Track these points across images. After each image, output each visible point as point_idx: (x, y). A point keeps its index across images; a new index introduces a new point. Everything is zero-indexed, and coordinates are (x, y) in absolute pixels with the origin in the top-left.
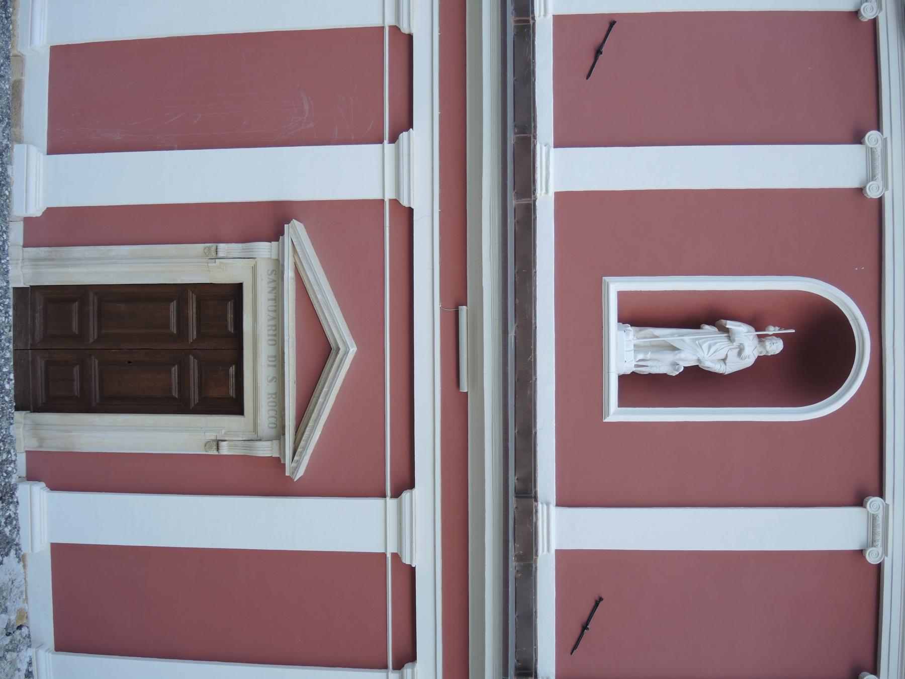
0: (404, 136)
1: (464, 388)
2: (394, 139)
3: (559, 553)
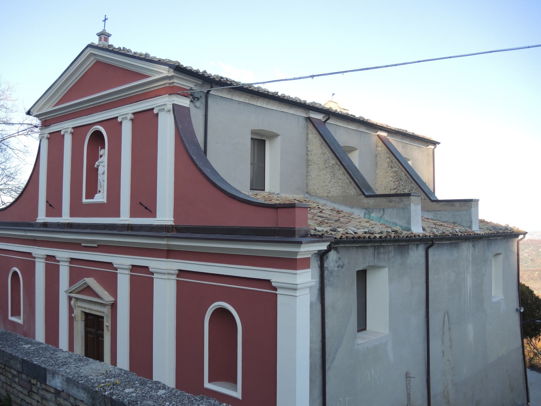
0: (115, 266)
1: (96, 245)
2: (275, 289)
3: (131, 217)
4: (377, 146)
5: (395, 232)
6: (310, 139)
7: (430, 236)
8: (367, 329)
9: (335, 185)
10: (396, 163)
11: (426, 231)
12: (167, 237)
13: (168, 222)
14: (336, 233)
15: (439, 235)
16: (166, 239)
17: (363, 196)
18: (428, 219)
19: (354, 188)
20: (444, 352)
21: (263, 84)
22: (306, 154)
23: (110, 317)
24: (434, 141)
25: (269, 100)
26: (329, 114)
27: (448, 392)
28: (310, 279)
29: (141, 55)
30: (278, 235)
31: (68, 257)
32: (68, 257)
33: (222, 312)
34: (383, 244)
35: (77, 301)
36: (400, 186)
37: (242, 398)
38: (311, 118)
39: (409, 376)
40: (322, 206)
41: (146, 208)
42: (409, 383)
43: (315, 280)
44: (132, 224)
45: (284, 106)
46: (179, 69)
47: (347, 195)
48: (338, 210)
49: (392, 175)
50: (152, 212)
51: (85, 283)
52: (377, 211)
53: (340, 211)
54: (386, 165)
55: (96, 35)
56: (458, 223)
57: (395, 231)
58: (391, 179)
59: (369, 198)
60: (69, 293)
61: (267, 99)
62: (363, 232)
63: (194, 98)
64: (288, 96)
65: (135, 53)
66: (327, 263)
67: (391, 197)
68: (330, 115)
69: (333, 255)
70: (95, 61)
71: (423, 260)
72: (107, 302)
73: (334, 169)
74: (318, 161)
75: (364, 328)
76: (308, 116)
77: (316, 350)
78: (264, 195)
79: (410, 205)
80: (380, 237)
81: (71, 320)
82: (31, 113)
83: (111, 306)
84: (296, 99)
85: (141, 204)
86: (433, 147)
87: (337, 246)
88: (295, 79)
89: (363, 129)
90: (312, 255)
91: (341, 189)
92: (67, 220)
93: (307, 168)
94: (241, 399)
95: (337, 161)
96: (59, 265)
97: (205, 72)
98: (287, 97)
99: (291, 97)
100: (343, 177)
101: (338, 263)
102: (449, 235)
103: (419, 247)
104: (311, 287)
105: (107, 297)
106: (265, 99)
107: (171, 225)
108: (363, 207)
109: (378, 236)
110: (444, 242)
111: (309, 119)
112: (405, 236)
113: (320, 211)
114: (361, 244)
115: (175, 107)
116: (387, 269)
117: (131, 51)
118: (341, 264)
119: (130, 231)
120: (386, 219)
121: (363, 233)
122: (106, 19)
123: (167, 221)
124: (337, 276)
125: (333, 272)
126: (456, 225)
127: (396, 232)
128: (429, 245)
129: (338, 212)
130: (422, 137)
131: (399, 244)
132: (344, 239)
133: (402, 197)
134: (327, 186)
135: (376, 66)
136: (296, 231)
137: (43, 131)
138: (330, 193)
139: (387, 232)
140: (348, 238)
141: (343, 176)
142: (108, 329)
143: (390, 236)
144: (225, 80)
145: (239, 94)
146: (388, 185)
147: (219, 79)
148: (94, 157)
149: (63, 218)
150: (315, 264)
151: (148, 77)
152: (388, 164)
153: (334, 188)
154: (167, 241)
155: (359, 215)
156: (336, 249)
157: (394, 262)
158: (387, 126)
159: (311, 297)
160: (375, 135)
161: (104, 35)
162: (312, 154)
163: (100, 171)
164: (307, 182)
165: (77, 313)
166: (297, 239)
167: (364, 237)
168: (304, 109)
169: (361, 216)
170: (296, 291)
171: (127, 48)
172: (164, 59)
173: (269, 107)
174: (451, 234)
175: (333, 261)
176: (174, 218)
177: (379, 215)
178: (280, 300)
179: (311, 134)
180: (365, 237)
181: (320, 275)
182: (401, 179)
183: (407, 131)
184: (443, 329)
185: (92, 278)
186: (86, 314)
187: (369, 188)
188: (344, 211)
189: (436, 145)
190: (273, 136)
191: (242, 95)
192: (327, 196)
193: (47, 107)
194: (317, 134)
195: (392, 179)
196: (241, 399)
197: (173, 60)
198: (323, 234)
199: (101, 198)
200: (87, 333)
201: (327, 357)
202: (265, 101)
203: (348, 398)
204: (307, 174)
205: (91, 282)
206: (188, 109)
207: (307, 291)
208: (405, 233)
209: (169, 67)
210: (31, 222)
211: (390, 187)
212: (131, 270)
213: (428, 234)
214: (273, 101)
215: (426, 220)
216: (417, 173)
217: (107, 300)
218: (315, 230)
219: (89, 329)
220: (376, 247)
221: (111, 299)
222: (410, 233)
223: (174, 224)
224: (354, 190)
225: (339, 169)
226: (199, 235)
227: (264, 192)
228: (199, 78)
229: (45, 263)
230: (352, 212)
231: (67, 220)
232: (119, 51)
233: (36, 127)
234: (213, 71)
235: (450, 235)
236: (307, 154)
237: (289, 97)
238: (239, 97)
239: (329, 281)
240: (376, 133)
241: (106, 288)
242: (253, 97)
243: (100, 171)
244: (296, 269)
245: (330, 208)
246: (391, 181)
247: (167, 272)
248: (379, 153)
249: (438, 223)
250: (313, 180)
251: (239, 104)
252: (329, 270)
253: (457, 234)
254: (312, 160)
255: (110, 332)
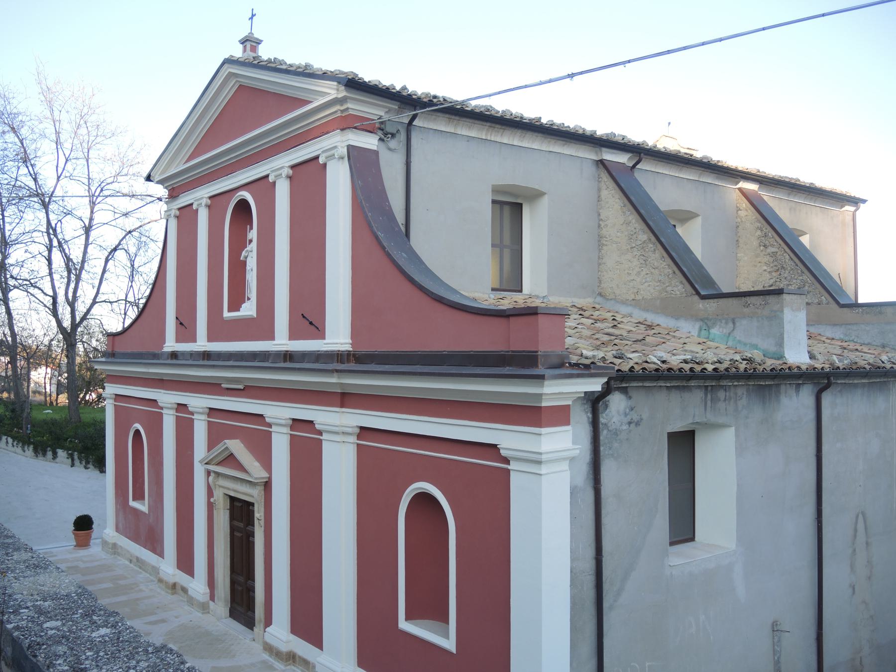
0: (267, 420)
1: (241, 387)
4: (739, 209)
5: (748, 361)
6: (603, 199)
7: (822, 368)
8: (696, 539)
9: (648, 279)
10: (773, 238)
11: (818, 359)
12: (337, 371)
13: (343, 346)
14: (623, 361)
15: (844, 366)
16: (335, 374)
17: (696, 298)
18: (833, 339)
19: (681, 282)
20: (854, 586)
21: (488, 98)
22: (597, 225)
23: (263, 503)
24: (854, 198)
25: (524, 132)
26: (640, 154)
27: (861, 661)
28: (572, 446)
29: (299, 67)
30: (510, 365)
31: (205, 406)
32: (174, 401)
33: (424, 500)
34: (724, 383)
35: (218, 476)
36: (780, 280)
37: (456, 651)
38: (605, 162)
39: (779, 628)
40: (622, 316)
41: (311, 323)
42: (779, 641)
43: (580, 446)
44: (291, 352)
45: (553, 141)
46: (354, 84)
47: (669, 296)
48: (650, 324)
49: (767, 260)
50: (319, 330)
51: (227, 447)
52: (722, 325)
53: (654, 325)
54: (756, 243)
55: (239, 43)
56: (891, 347)
57: (748, 358)
58: (765, 268)
59: (707, 300)
60: (206, 464)
61: (520, 131)
62: (681, 361)
63: (386, 134)
64: (560, 124)
65: (291, 66)
66: (606, 415)
67: (748, 298)
68: (642, 154)
69: (617, 402)
70: (238, 86)
71: (811, 415)
72: (256, 478)
73: (645, 251)
74: (619, 237)
75: (691, 536)
76: (601, 159)
77: (584, 572)
78: (517, 300)
79: (782, 311)
80: (715, 370)
81: (210, 507)
82: (151, 178)
83: (265, 487)
84: (577, 129)
85: (304, 317)
86: (852, 209)
87: (627, 385)
88: (541, 83)
89: (709, 178)
90: (574, 401)
91: (658, 286)
92: (203, 346)
93: (600, 251)
94: (455, 653)
95: (651, 235)
96: (193, 419)
97: (404, 88)
98: (557, 126)
99: (565, 125)
100: (661, 264)
101: (628, 416)
102: (864, 368)
103: (801, 389)
104: (572, 460)
105: (257, 471)
106: (516, 130)
107: (347, 351)
108: (694, 317)
109: (710, 367)
110: (856, 381)
111: (602, 163)
112: (768, 369)
113: (613, 325)
114: (676, 383)
115: (350, 151)
116: (733, 429)
117: (286, 63)
118: (635, 417)
119: (288, 363)
120: (738, 338)
121: (681, 362)
122: (253, 15)
123: (342, 344)
124: (627, 439)
125: (619, 433)
126: (887, 349)
127: (749, 360)
128: (824, 385)
129: (650, 327)
130: (829, 190)
131: (759, 383)
132: (637, 372)
133: (767, 297)
134: (634, 281)
135: (685, 46)
136: (539, 357)
137: (169, 205)
138: (638, 293)
139: (731, 360)
140: (646, 370)
141: (662, 262)
142: (259, 523)
143: (735, 368)
144: (440, 101)
145: (468, 123)
146: (759, 278)
147: (428, 99)
148: (239, 243)
149: (197, 344)
150: (581, 418)
151: (308, 102)
152: (759, 241)
153: (646, 284)
154: (339, 378)
155: (690, 332)
156: (624, 391)
157: (747, 417)
158: (759, 171)
159: (572, 478)
160: (732, 190)
161: (252, 43)
162: (607, 225)
163: (249, 266)
164: (600, 275)
165: (219, 495)
166: (540, 371)
167: (680, 370)
168: (593, 145)
169: (692, 334)
170: (541, 464)
171: (280, 57)
172: (332, 71)
173: (525, 144)
174: (870, 366)
175: (618, 412)
176: (352, 338)
177: (726, 331)
178: (516, 482)
179: (606, 189)
180: (682, 368)
181: (591, 438)
182: (783, 267)
183: (799, 180)
184: (853, 544)
185: (238, 441)
186: (233, 499)
187: (709, 281)
188: (663, 325)
189: (859, 204)
190: (535, 195)
191: (473, 125)
192: (633, 300)
193: (175, 165)
194: (615, 190)
195: (766, 268)
196: (455, 652)
197: (346, 70)
198: (593, 363)
199: (249, 309)
200: (233, 529)
201: (606, 587)
202: (515, 134)
203: (650, 663)
204: (600, 261)
205: (236, 446)
206: (376, 153)
207: (565, 466)
208: (770, 363)
209: (337, 82)
210: (156, 352)
211: (763, 282)
212: (292, 428)
213: (818, 366)
214: (531, 133)
215: (829, 341)
216: (813, 254)
217: (256, 476)
218: (582, 355)
219: (236, 523)
220: (709, 388)
221: (262, 474)
222: (781, 362)
223: (351, 349)
224: (681, 287)
225: (655, 250)
226: (387, 366)
227: (519, 295)
228: (392, 99)
229: (175, 417)
230: (678, 327)
231: (203, 346)
232: (268, 64)
233: (160, 199)
234: (418, 87)
235: (868, 367)
236: (599, 226)
237: (562, 125)
238: (467, 129)
239: (610, 448)
240: (736, 185)
241: (258, 458)
242: (494, 127)
243: (249, 266)
244: (540, 426)
245: (637, 319)
246: (765, 270)
247: (341, 431)
248: (742, 221)
249: (851, 347)
250: (610, 271)
251: (468, 141)
252: (610, 428)
253: (883, 365)
254: (607, 236)
255: (263, 529)
